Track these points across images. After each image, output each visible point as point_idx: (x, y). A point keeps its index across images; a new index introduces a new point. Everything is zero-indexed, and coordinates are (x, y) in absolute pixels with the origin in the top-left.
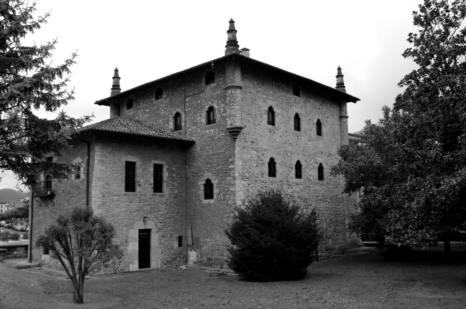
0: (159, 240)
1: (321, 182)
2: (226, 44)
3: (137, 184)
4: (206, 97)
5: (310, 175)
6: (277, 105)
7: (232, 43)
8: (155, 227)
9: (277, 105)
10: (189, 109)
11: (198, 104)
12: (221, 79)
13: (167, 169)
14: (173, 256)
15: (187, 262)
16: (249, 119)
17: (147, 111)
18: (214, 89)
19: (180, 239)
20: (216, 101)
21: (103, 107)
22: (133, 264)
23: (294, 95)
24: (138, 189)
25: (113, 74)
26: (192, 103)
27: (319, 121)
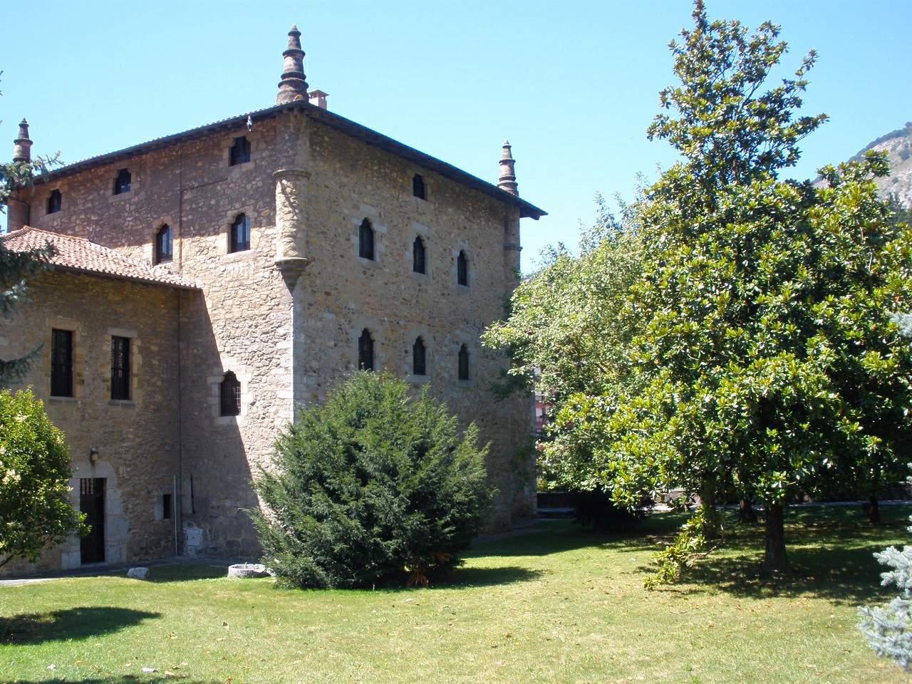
0: (124, 502)
1: (464, 383)
2: (281, 80)
3: (75, 379)
4: (229, 192)
5: (441, 368)
6: (380, 215)
7: (296, 79)
8: (115, 475)
9: (380, 215)
10: (190, 217)
11: (210, 207)
12: (264, 155)
13: (141, 350)
14: (153, 538)
15: (182, 551)
16: (323, 244)
17: (93, 218)
18: (248, 177)
19: (167, 499)
20: (253, 202)
22: (68, 553)
23: (415, 195)
24: (78, 390)
25: (16, 133)
26: (197, 204)
27: (462, 254)
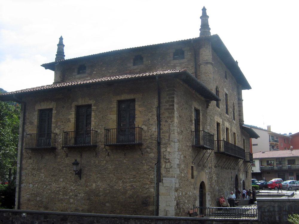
7: (205, 26)
21: (49, 71)
